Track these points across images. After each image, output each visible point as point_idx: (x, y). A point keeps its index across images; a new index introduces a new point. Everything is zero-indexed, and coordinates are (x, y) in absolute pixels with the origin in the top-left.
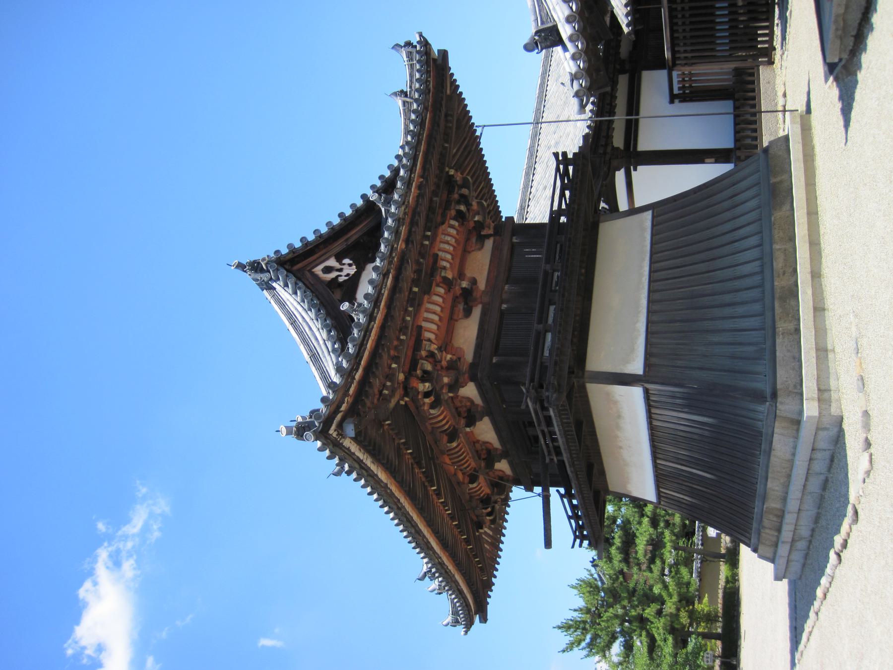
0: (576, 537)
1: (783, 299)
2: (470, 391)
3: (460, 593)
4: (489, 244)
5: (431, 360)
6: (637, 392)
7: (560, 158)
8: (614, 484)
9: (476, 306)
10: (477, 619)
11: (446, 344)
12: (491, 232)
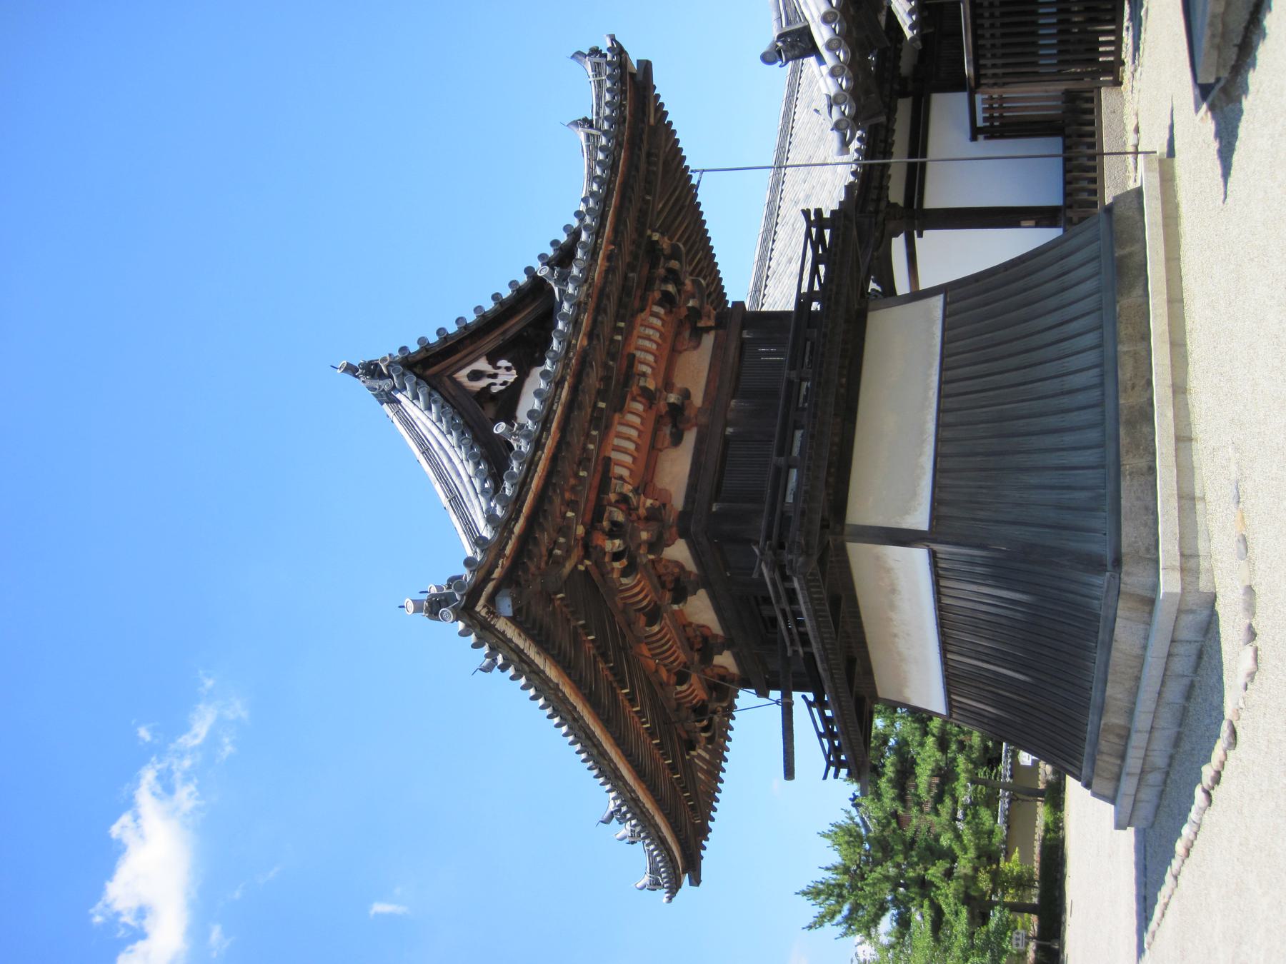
0: (829, 764)
1: (1131, 424)
2: (679, 551)
3: (661, 843)
4: (708, 340)
5: (623, 506)
6: (918, 558)
7: (813, 218)
8: (885, 688)
9: (689, 429)
11: (645, 485)
12: (712, 323)
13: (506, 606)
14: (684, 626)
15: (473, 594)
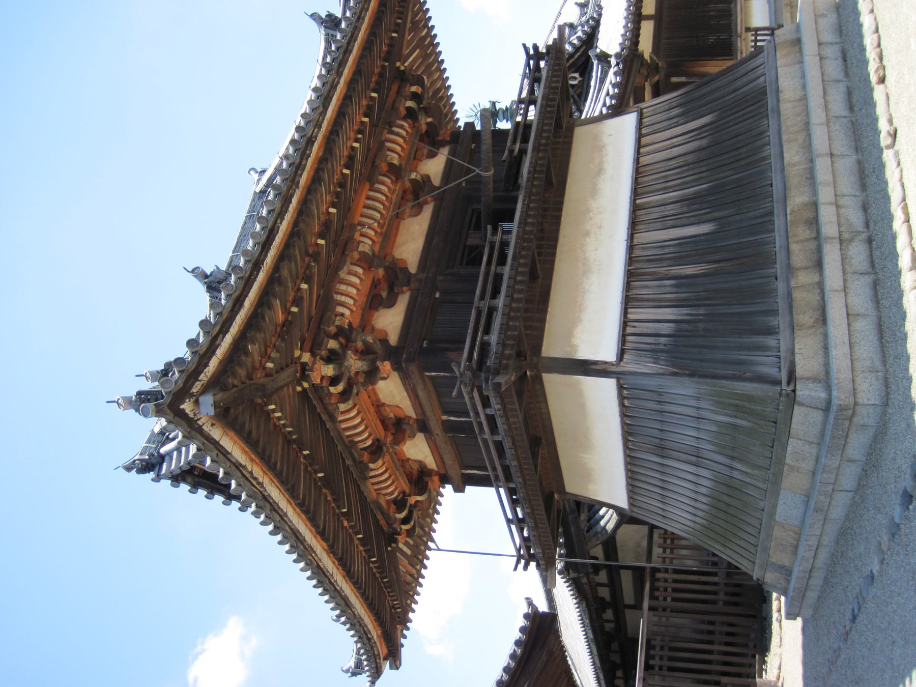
0: (519, 557)
6: (608, 386)
7: (532, 52)
9: (403, 292)
10: (387, 665)
13: (207, 400)
14: (404, 462)
15: (182, 393)
